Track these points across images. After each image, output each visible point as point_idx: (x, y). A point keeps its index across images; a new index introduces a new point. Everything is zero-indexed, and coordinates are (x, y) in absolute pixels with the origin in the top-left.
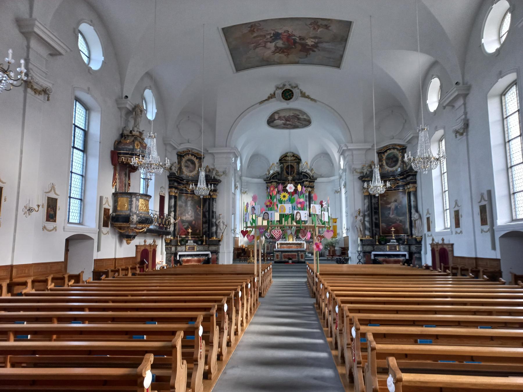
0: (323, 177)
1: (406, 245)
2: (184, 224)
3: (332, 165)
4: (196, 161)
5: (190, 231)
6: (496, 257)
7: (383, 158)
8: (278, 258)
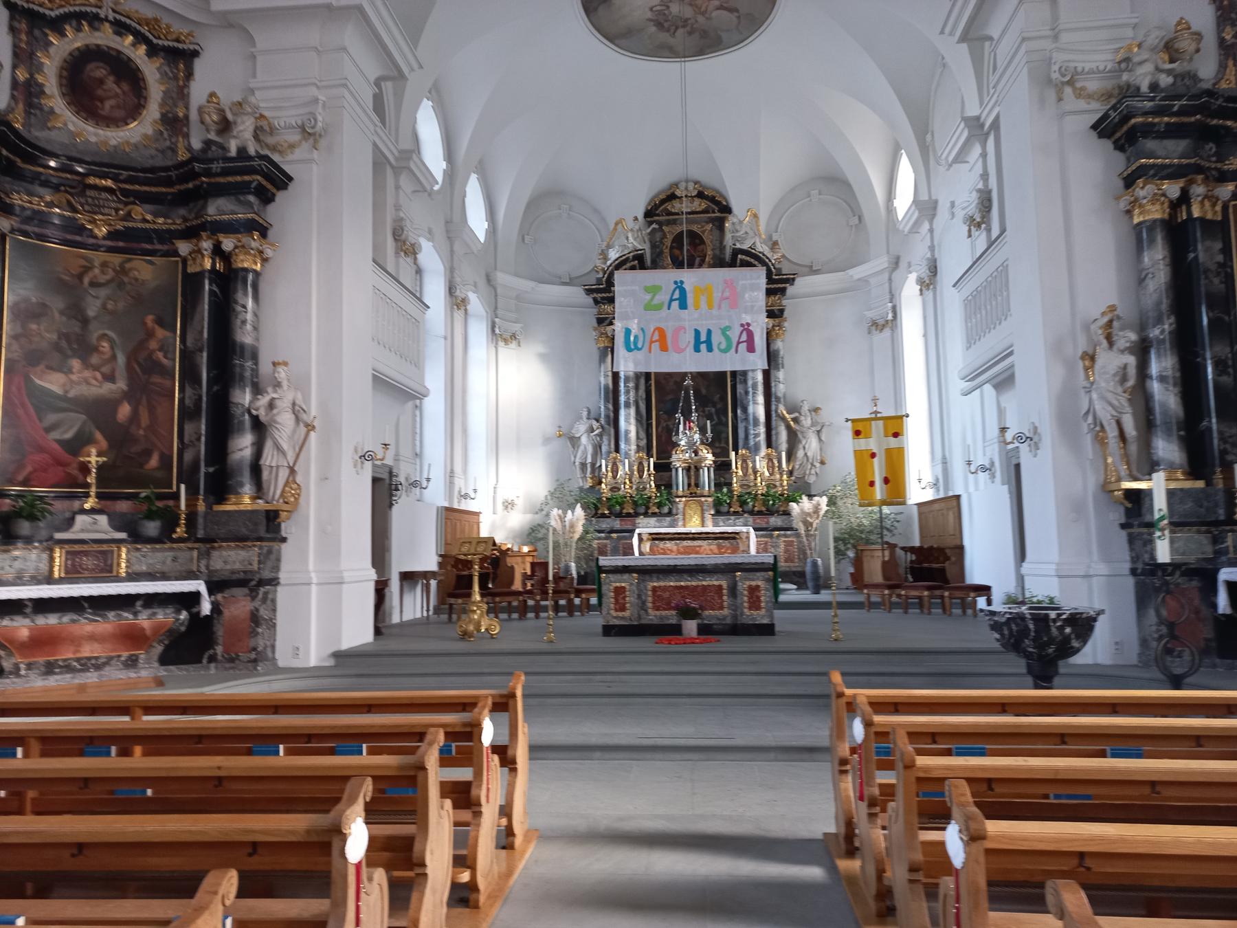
0: (817, 272)
2: (52, 418)
3: (856, 220)
4: (150, 70)
5: (94, 459)
8: (623, 609)
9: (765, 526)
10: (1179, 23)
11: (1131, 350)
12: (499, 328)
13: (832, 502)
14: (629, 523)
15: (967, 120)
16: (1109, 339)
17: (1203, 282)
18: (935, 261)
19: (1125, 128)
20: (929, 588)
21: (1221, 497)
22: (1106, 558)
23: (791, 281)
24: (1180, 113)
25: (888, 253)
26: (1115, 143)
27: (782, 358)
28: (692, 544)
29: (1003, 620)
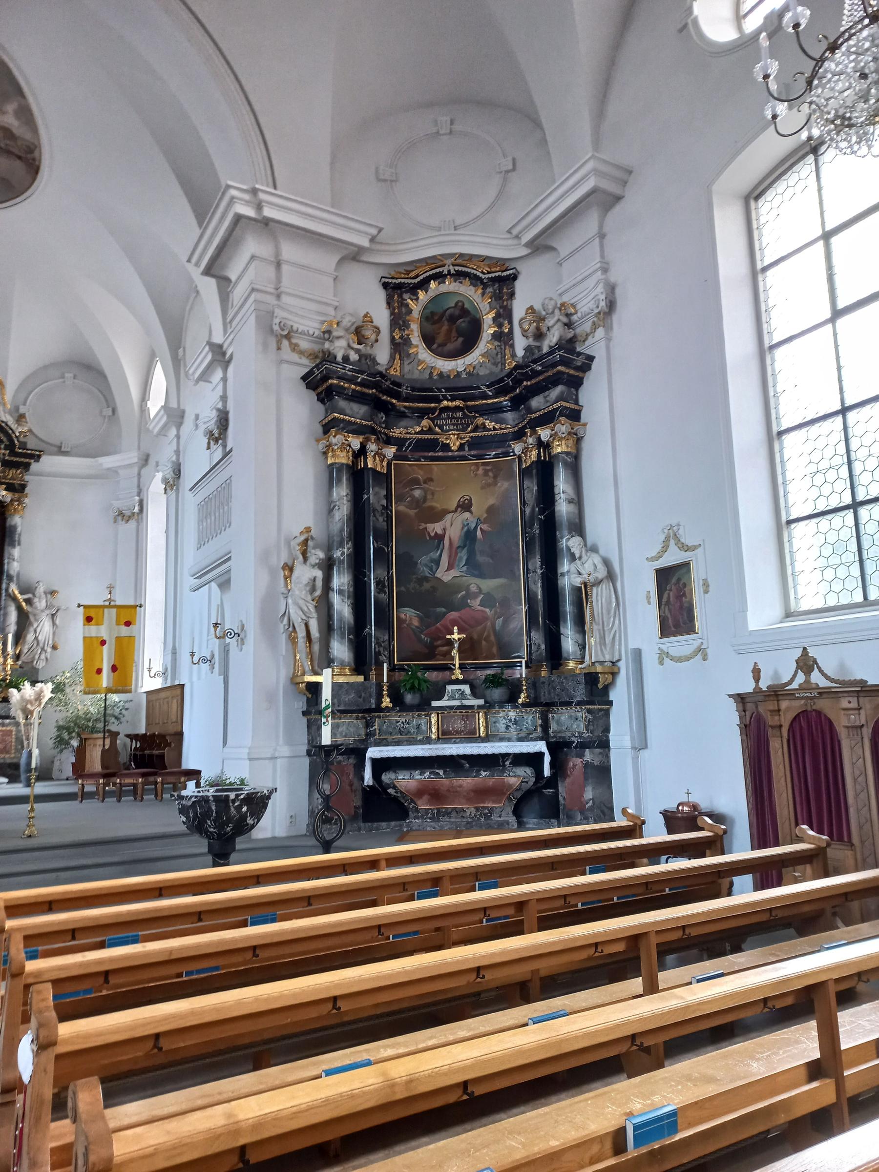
0: (66, 453)
1: (524, 705)
6: (615, 748)
7: (410, 311)
10: (366, 316)
11: (319, 566)
13: (58, 688)
15: (210, 344)
16: (304, 554)
17: (371, 518)
18: (180, 465)
19: (325, 386)
20: (143, 775)
21: (373, 690)
22: (290, 742)
23: (37, 458)
24: (362, 384)
25: (139, 448)
26: (318, 395)
27: (20, 535)
29: (190, 803)
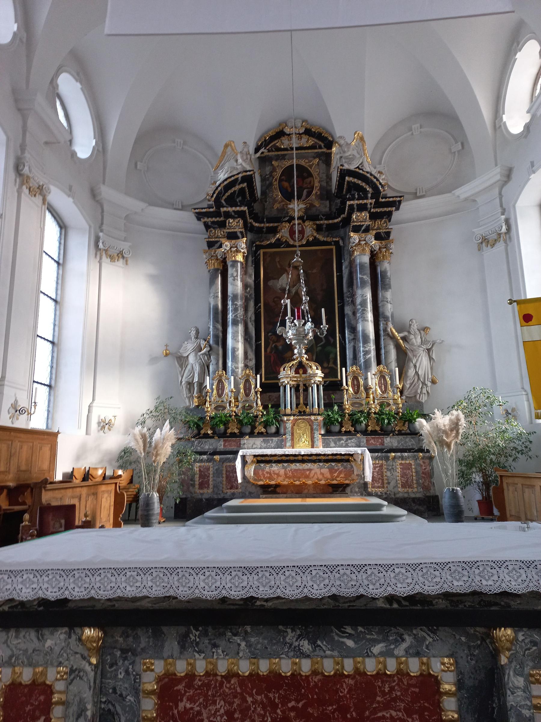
0: (405, 223)
9: (379, 447)
12: (103, 243)
14: (233, 443)
23: (396, 204)
28: (301, 468)
